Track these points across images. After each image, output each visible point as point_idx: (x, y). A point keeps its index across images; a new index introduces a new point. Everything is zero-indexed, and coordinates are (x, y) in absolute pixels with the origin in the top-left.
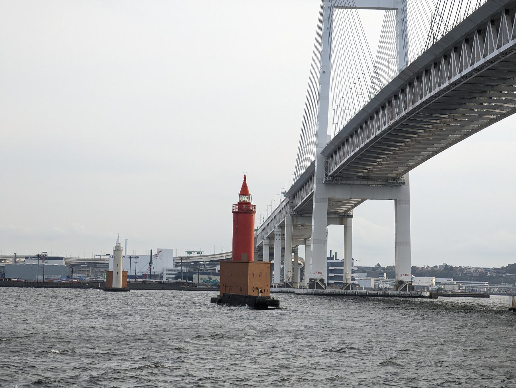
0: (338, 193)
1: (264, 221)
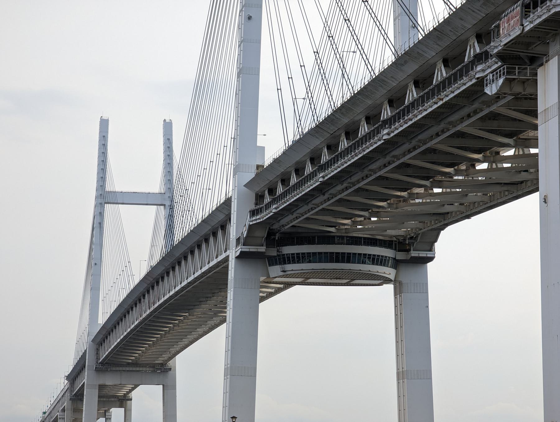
0: (109, 380)
1: (51, 404)
